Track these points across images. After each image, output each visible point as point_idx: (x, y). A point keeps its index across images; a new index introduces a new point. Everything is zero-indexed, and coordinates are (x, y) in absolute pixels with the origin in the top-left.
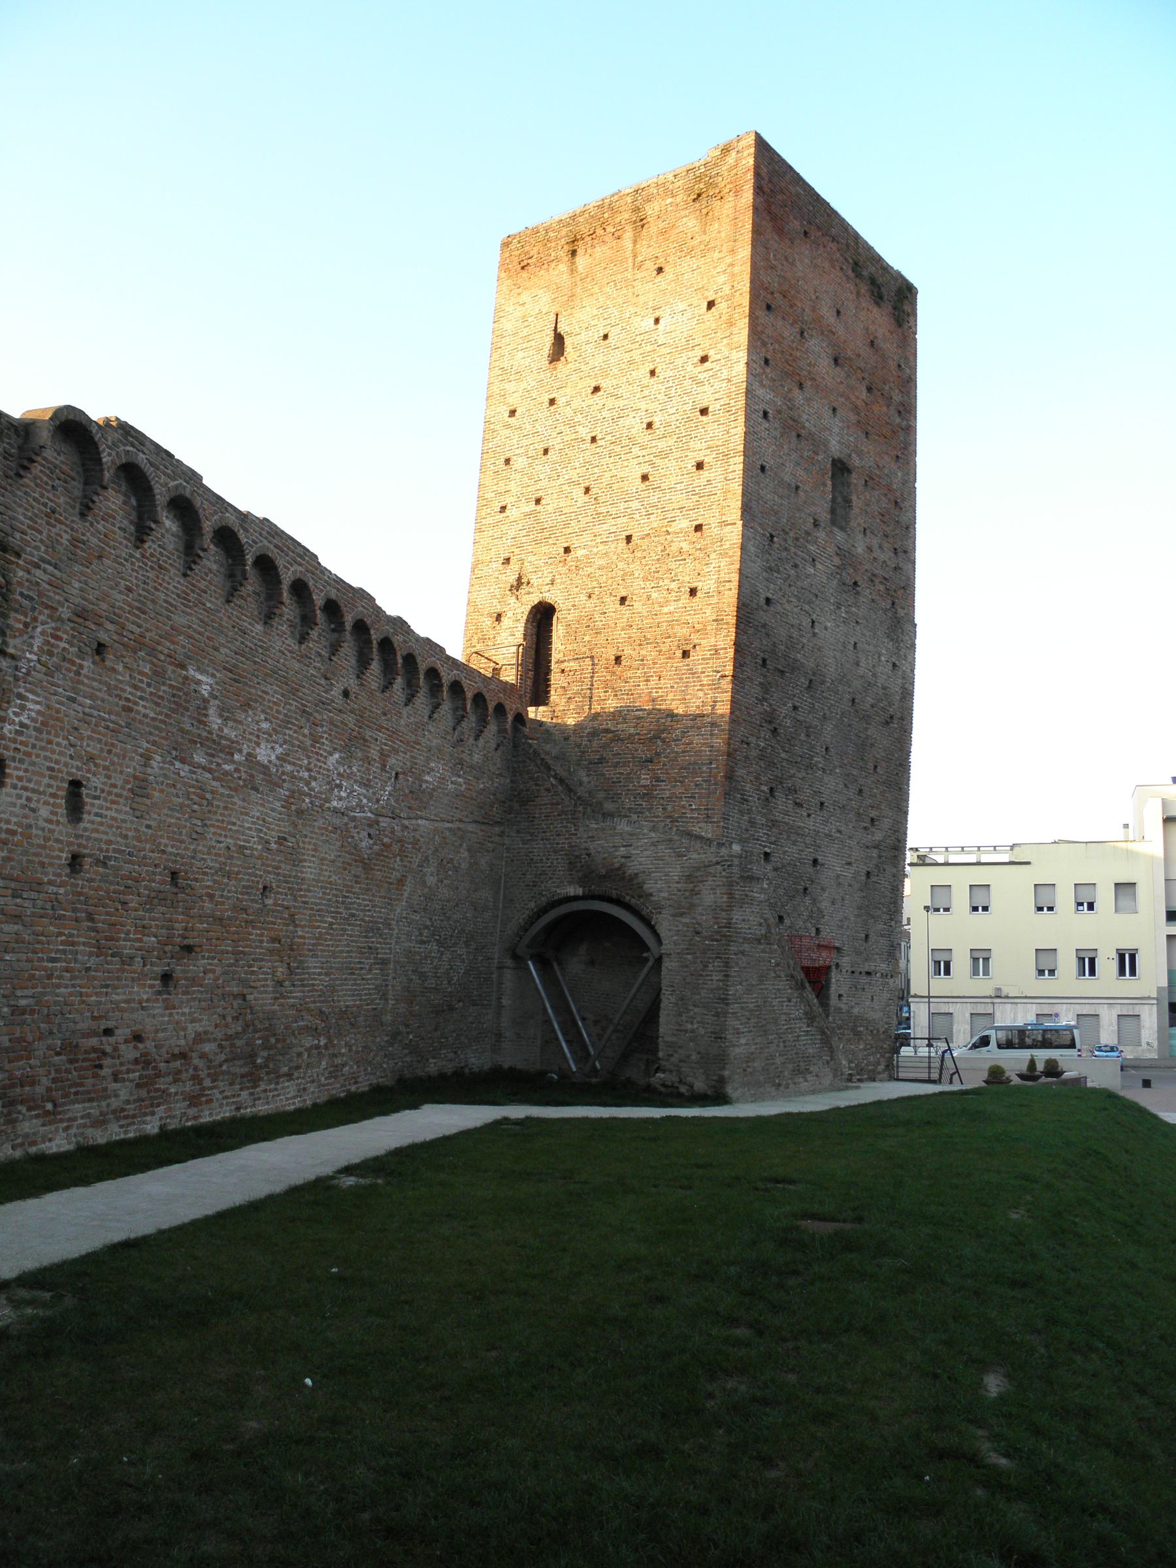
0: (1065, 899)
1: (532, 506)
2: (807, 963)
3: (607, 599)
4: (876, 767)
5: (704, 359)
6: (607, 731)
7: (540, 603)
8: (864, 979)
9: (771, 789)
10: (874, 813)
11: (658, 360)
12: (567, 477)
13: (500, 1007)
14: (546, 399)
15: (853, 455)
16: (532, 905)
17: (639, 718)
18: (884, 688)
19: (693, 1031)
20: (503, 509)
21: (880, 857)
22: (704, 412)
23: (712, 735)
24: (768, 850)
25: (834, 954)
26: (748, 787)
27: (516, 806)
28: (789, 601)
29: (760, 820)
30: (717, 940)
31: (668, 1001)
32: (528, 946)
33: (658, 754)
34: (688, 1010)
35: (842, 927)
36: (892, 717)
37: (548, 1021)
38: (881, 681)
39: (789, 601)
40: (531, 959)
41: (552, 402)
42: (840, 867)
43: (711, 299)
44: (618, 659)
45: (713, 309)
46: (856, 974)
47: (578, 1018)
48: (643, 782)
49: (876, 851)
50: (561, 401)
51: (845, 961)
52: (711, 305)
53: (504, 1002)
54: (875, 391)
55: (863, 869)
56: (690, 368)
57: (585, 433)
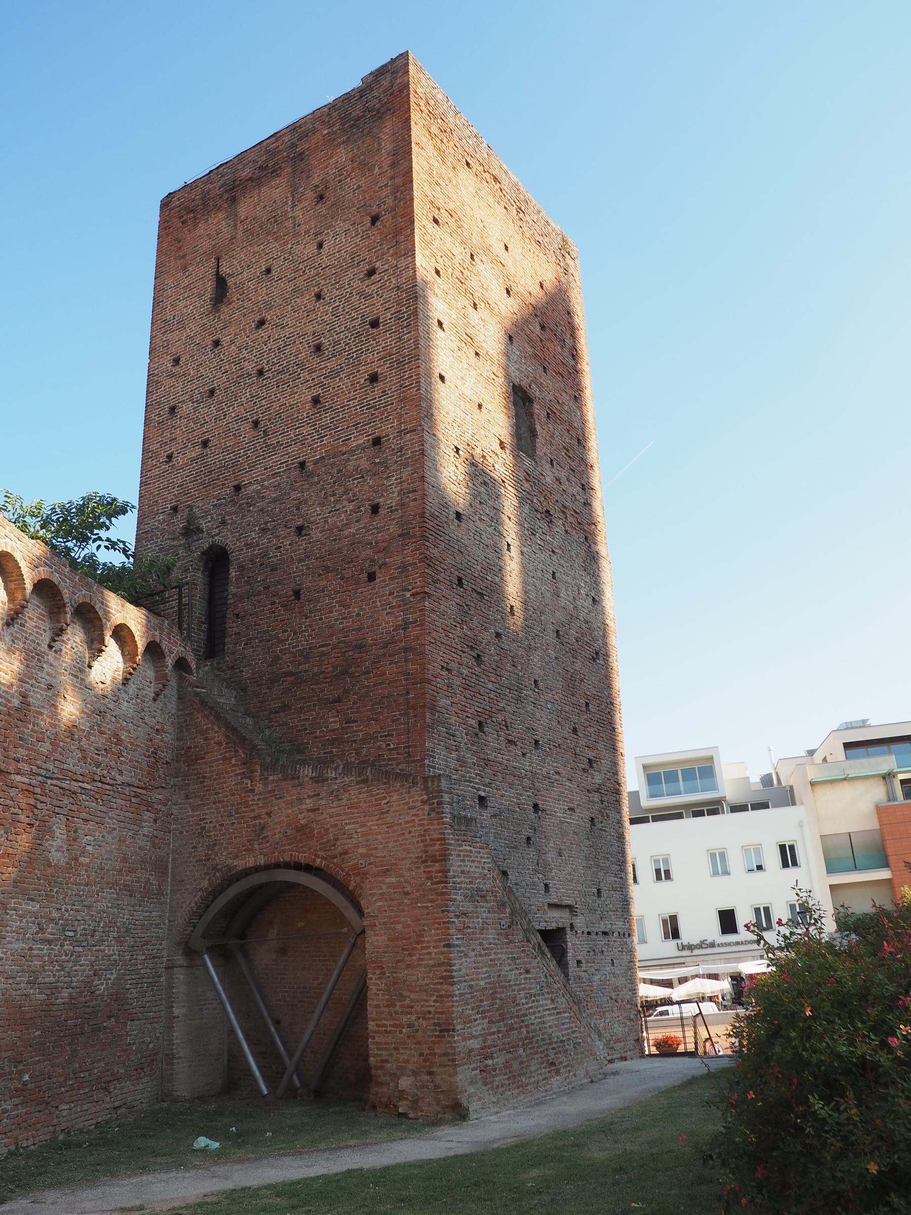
0: (736, 862)
1: (199, 449)
2: (542, 926)
3: (282, 532)
4: (587, 704)
5: (371, 273)
6: (289, 674)
7: (211, 548)
8: (602, 941)
9: (480, 723)
10: (591, 754)
11: (323, 282)
12: (233, 415)
13: (171, 1018)
14: (209, 341)
15: (533, 385)
16: (206, 883)
17: (322, 654)
18: (587, 622)
19: (410, 1026)
20: (170, 457)
21: (602, 802)
22: (375, 324)
23: (406, 661)
24: (483, 794)
25: (566, 914)
26: (453, 720)
27: (185, 768)
28: (480, 519)
29: (470, 759)
30: (431, 901)
31: (376, 985)
32: (203, 937)
33: (346, 692)
34: (403, 997)
35: (571, 881)
36: (597, 653)
37: (232, 1031)
38: (582, 615)
39: (480, 519)
40: (210, 950)
41: (217, 343)
42: (564, 808)
43: (374, 213)
44: (297, 594)
45: (378, 223)
46: (593, 936)
47: (269, 1021)
48: (333, 726)
49: (597, 795)
50: (225, 341)
51: (580, 922)
52: (375, 219)
53: (176, 1011)
54: (548, 329)
55: (586, 814)
56: (356, 283)
57: (250, 367)
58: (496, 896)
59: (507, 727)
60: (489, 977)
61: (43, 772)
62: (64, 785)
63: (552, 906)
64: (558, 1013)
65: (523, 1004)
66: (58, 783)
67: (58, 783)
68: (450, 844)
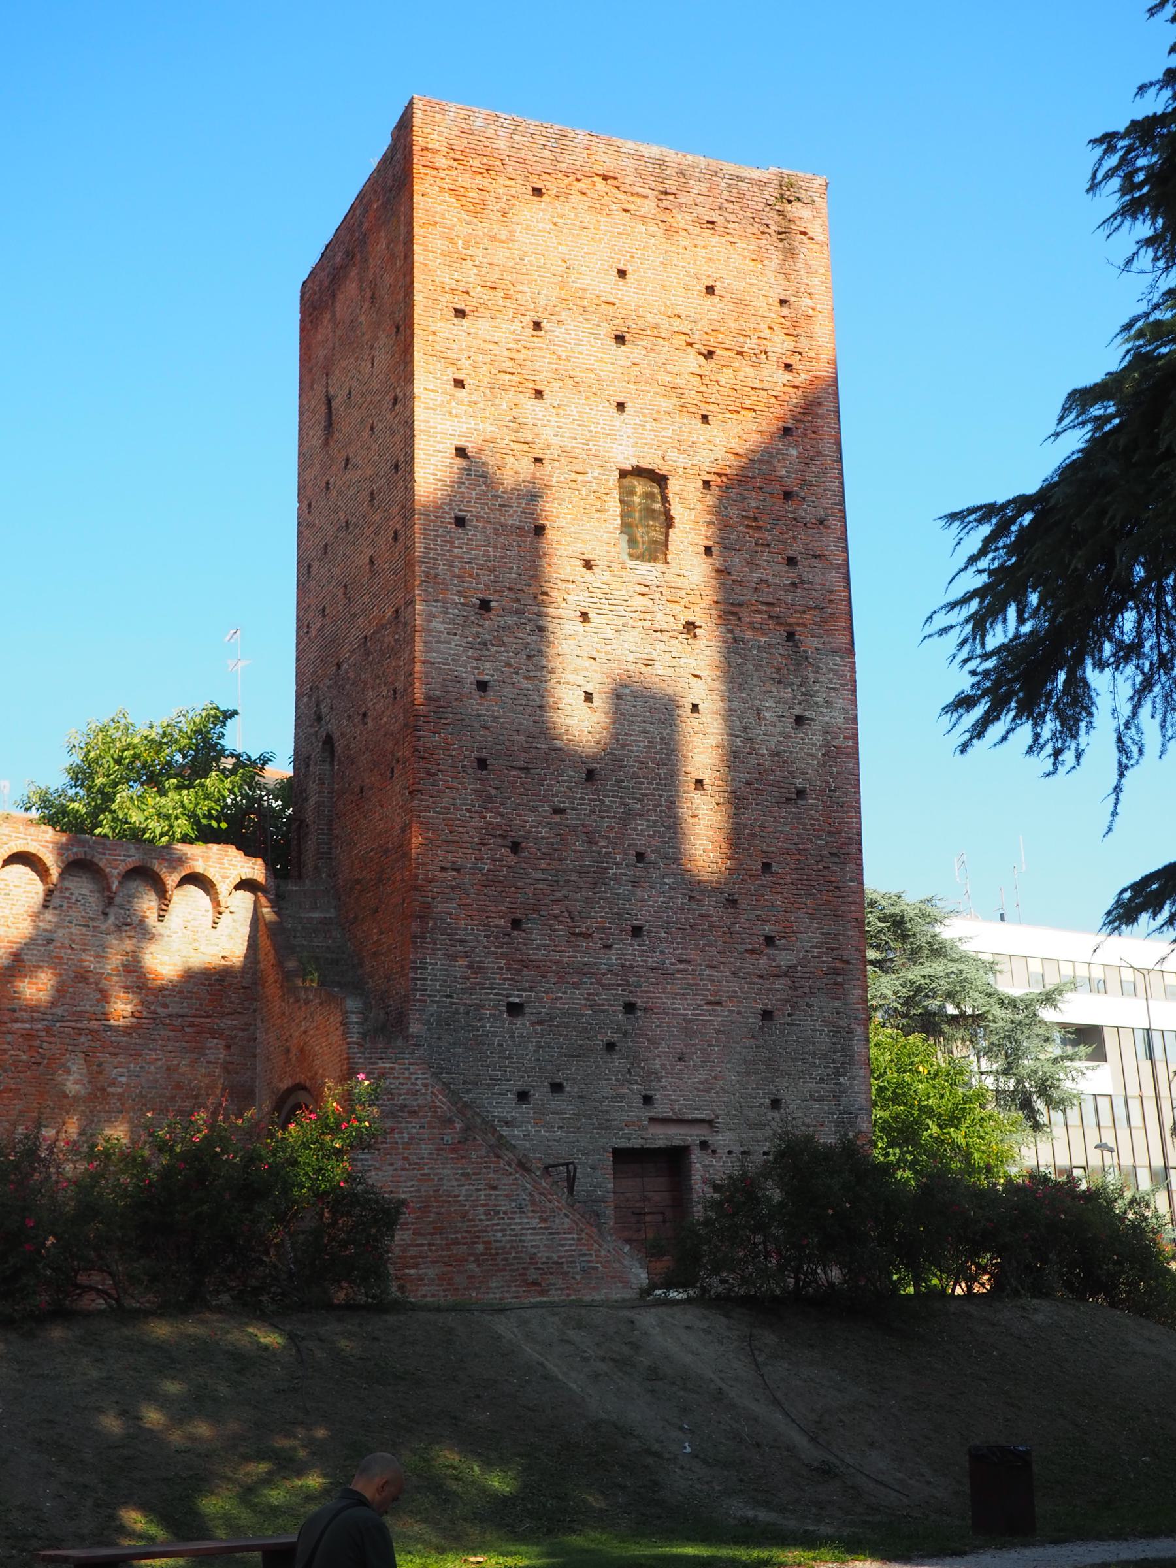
58: (436, 1112)
59: (572, 918)
60: (419, 1191)
61: (50, 1017)
62: (79, 1025)
63: (653, 1120)
64: (551, 1234)
65: (480, 1220)
66: (73, 1024)
67: (73, 1024)
68: (357, 1063)
